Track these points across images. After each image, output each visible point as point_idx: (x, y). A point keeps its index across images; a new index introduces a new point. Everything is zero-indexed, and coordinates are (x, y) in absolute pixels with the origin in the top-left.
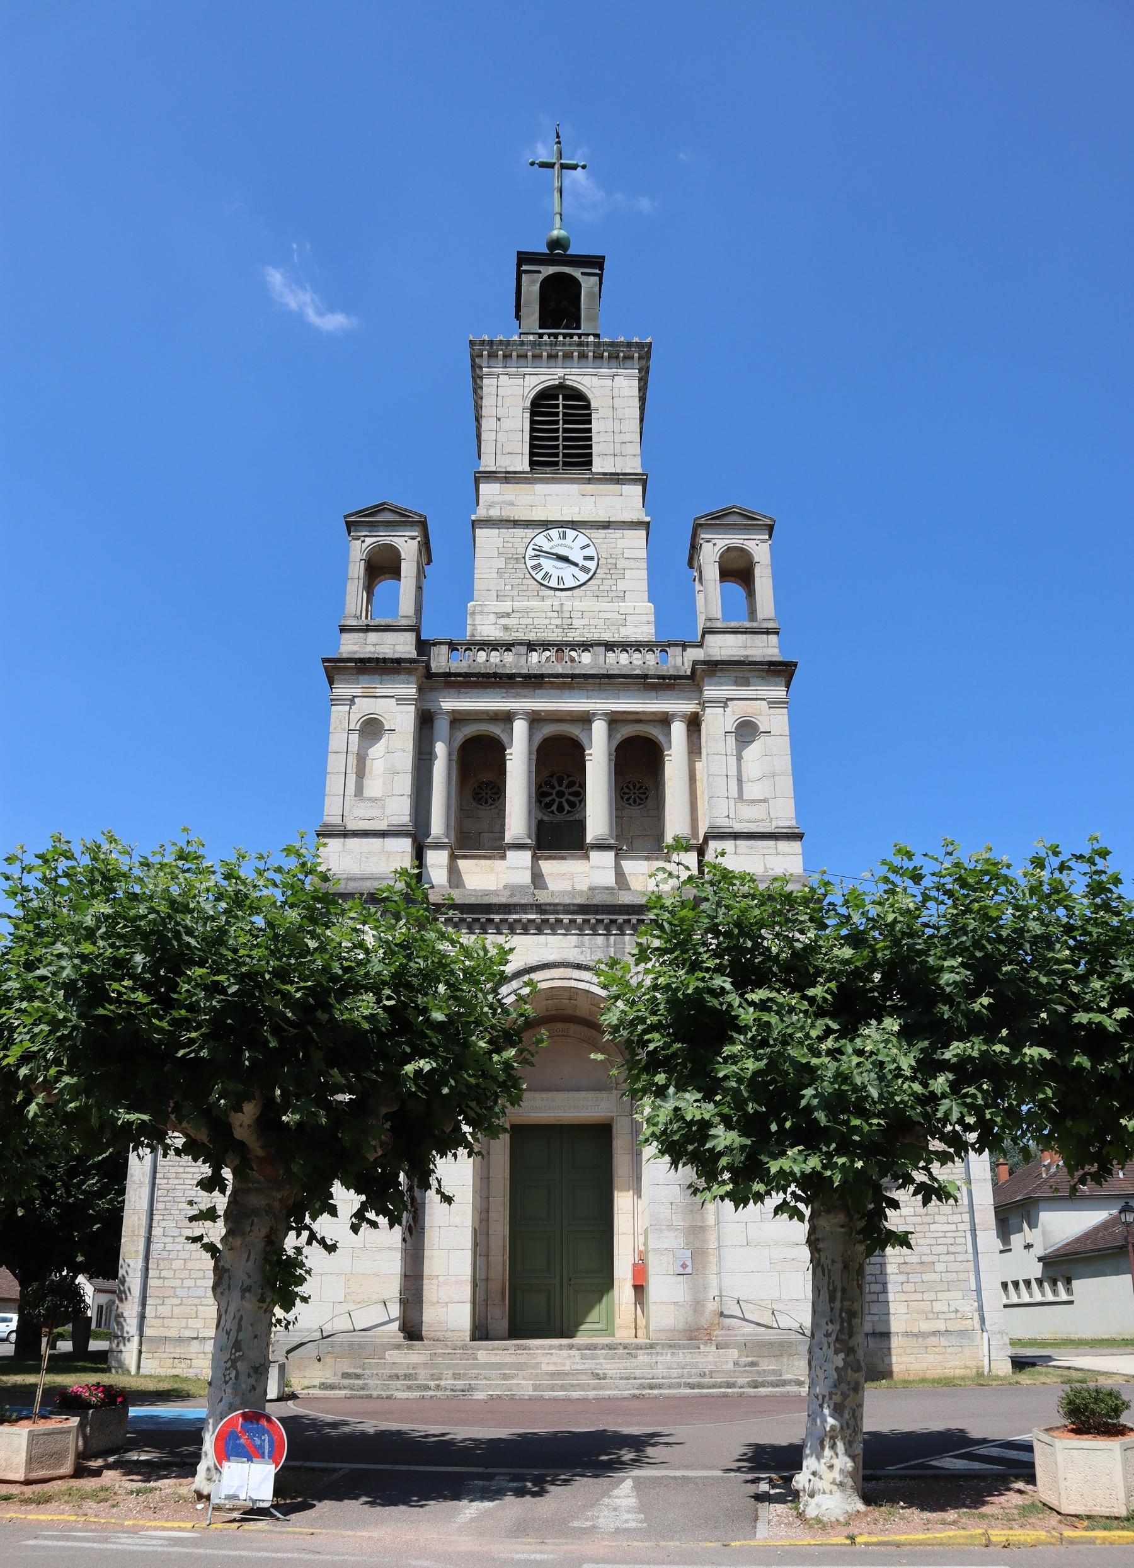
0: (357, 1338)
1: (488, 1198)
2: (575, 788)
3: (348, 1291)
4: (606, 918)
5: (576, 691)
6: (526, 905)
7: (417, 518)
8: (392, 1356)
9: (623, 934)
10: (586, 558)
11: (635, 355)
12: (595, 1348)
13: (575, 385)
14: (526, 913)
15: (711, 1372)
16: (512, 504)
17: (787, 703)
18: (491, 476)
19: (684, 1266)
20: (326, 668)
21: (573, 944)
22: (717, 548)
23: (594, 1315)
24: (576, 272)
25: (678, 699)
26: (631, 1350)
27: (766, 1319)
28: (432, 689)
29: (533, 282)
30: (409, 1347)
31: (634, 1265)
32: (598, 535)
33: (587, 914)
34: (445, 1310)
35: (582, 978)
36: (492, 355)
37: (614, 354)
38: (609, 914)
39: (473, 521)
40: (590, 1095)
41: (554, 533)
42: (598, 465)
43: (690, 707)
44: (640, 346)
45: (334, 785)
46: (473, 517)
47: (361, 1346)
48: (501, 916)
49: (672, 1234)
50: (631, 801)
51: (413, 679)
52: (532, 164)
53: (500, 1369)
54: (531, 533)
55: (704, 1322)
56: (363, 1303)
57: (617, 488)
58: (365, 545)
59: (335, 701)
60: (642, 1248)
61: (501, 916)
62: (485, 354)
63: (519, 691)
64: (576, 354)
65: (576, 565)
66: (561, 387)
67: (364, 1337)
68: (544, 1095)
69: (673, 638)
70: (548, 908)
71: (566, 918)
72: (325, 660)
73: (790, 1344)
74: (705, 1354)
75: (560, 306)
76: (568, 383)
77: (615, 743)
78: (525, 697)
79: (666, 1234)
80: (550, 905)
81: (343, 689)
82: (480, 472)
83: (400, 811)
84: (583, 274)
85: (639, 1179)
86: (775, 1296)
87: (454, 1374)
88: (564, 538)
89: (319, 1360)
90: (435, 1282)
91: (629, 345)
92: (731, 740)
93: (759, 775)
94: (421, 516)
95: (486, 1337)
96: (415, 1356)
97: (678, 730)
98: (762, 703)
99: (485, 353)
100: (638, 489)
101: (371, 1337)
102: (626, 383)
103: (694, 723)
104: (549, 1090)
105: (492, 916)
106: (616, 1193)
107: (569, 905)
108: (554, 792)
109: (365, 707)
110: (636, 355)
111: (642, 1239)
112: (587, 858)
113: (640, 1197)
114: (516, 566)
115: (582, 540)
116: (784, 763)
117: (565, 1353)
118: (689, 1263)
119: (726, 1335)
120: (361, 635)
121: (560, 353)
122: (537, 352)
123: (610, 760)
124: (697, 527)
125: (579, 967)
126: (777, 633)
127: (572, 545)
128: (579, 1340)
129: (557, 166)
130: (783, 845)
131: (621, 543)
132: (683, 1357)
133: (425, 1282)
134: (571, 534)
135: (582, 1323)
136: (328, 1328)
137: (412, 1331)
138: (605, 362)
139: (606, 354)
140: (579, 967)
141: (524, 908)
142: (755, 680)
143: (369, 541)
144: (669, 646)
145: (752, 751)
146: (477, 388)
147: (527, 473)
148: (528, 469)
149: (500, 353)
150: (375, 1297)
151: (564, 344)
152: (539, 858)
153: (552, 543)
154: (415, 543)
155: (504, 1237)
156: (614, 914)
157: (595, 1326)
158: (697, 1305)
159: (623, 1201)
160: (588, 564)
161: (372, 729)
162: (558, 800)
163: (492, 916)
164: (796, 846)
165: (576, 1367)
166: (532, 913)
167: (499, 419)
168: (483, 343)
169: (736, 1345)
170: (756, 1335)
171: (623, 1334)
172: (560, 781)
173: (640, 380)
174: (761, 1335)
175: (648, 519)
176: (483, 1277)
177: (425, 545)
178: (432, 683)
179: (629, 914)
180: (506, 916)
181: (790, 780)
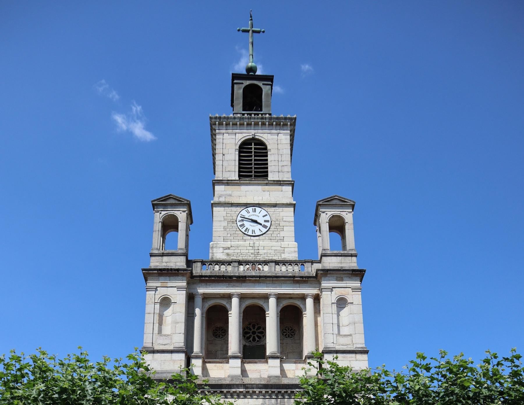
2: (261, 330)
4: (276, 391)
5: (261, 284)
6: (238, 385)
7: (186, 202)
10: (265, 221)
11: (288, 123)
13: (260, 138)
14: (239, 388)
16: (230, 195)
18: (220, 182)
20: (143, 273)
21: (261, 403)
22: (327, 216)
24: (260, 84)
25: (310, 287)
28: (193, 283)
33: (267, 389)
36: (221, 124)
37: (278, 123)
38: (278, 389)
39: (212, 204)
41: (250, 209)
42: (271, 177)
43: (315, 291)
44: (291, 119)
45: (148, 328)
46: (212, 202)
51: (185, 278)
52: (239, 30)
54: (239, 209)
59: (148, 289)
62: (217, 124)
64: (260, 123)
65: (261, 224)
66: (253, 139)
70: (249, 386)
71: (257, 391)
72: (143, 270)
76: (256, 137)
81: (152, 284)
82: (215, 180)
83: (179, 341)
84: (263, 84)
91: (286, 118)
92: (335, 306)
93: (347, 323)
94: (188, 201)
97: (309, 302)
98: (349, 289)
99: (217, 123)
100: (290, 188)
102: (284, 137)
103: (317, 299)
105: (223, 390)
107: (259, 384)
108: (251, 332)
109: (162, 292)
110: (289, 123)
112: (267, 362)
114: (232, 225)
115: (264, 212)
116: (359, 318)
120: (160, 257)
122: (242, 122)
124: (318, 206)
126: (356, 256)
129: (250, 32)
130: (359, 356)
131: (282, 214)
134: (258, 209)
138: (274, 127)
139: (274, 123)
141: (238, 386)
143: (163, 213)
144: (305, 262)
145: (344, 312)
148: (238, 179)
149: (224, 123)
151: (254, 118)
152: (244, 363)
154: (185, 214)
156: (280, 389)
160: (266, 224)
161: (166, 302)
163: (223, 390)
164: (365, 357)
166: (241, 388)
167: (224, 155)
168: (216, 118)
172: (254, 327)
173: (291, 136)
175: (294, 202)
177: (190, 215)
179: (287, 389)
180: (229, 390)
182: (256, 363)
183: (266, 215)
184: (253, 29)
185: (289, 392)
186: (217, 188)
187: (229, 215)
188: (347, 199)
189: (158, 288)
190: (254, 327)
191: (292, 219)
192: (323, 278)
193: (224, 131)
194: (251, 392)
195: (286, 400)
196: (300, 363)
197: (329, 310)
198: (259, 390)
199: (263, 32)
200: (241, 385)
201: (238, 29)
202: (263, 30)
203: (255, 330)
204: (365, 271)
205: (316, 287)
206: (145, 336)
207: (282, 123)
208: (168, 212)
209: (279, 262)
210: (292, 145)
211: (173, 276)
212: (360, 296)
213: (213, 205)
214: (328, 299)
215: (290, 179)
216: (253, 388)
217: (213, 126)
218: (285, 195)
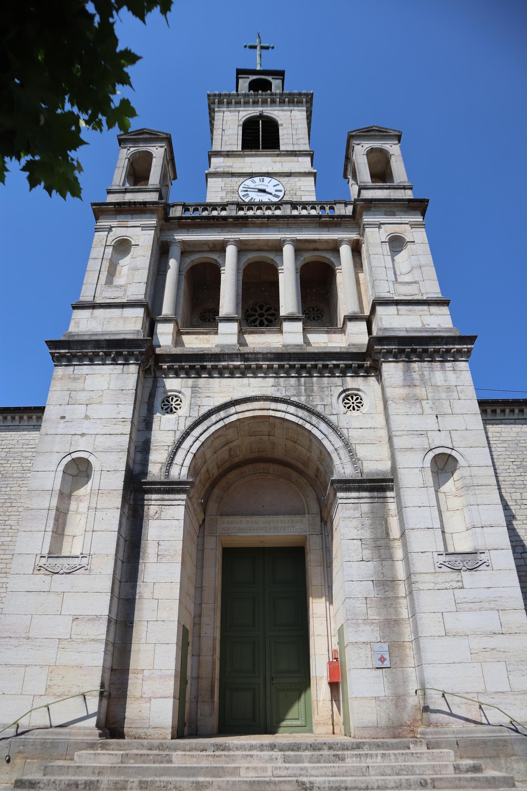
0: (50, 736)
1: (201, 604)
2: (272, 311)
3: (49, 683)
4: (297, 364)
5: (271, 229)
6: (232, 354)
7: (164, 136)
8: (85, 758)
9: (311, 376)
10: (276, 191)
11: (305, 100)
12: (299, 749)
13: (269, 115)
14: (233, 361)
15: (433, 780)
16: (231, 167)
17: (424, 225)
18: (218, 154)
19: (382, 659)
20: (94, 210)
21: (271, 384)
22: (364, 148)
23: (293, 712)
24: (269, 78)
25: (344, 232)
26: (336, 751)
27: (475, 714)
28: (169, 229)
29: (245, 82)
30: (103, 747)
31: (330, 663)
32: (285, 180)
33: (282, 361)
34: (148, 705)
35: (279, 408)
36: (221, 103)
37: (291, 100)
38: (300, 360)
39: (207, 174)
40: (287, 518)
41: (257, 179)
42: (282, 148)
43: (354, 236)
44: (306, 95)
45: (90, 278)
46: (206, 172)
47: (54, 745)
48: (212, 364)
49: (368, 628)
50: (312, 318)
51: (155, 216)
52: (245, 47)
53: (194, 775)
54: (241, 179)
55: (406, 718)
56: (63, 697)
57: (295, 159)
58: (129, 152)
59: (97, 230)
60: (336, 647)
61: (212, 364)
62: (216, 101)
63: (230, 229)
64: (269, 100)
65: (271, 194)
66: (261, 116)
67: (59, 734)
68: (249, 519)
69: (337, 199)
70: (250, 356)
71: (265, 364)
72: (93, 204)
73: (505, 742)
74: (418, 756)
75: (260, 85)
76: (264, 114)
77: (300, 264)
78: (235, 232)
79: (363, 627)
80: (252, 354)
81: (104, 223)
82: (211, 152)
83: (138, 290)
84: (272, 78)
85: (330, 588)
86: (480, 688)
87: (140, 782)
88: (263, 181)
89: (8, 761)
90: (140, 676)
91: (300, 94)
92: (386, 247)
93: (408, 269)
94: (167, 134)
95: (195, 734)
96: (108, 756)
97: (345, 251)
98: (405, 225)
99: (216, 100)
100: (309, 159)
101: (67, 734)
102: (299, 115)
103: (356, 249)
104: (253, 514)
105: (205, 364)
106: (311, 599)
107: (267, 353)
108: (257, 314)
109: (118, 233)
110: (304, 100)
111: (335, 640)
112: (281, 331)
113: (331, 603)
114: (232, 195)
115: (274, 182)
116: (427, 259)
117: (266, 754)
118: (387, 656)
119: (436, 733)
120: (121, 195)
121: (260, 100)
122: (247, 99)
123: (297, 273)
124: (351, 137)
125: (276, 400)
126: (411, 189)
127: (268, 184)
128: (281, 738)
129: (258, 48)
130: (434, 309)
131: (299, 184)
132: (395, 759)
133: (131, 676)
134: (267, 179)
135: (283, 720)
136: (24, 723)
137: (112, 726)
138: (286, 104)
139: (287, 99)
140: (276, 400)
141: (231, 356)
142: (398, 211)
143: (132, 149)
144: (335, 204)
145: (402, 257)
146: (212, 119)
147: (240, 151)
148: (240, 148)
149: (225, 100)
150: (76, 690)
151: (262, 95)
152: (244, 333)
153: (256, 184)
154: (163, 150)
155: (214, 639)
156: (304, 361)
157: (295, 723)
158: (398, 699)
159: (317, 607)
160: (278, 193)
161: (123, 246)
162: (259, 319)
163: (205, 364)
164: (445, 310)
165: (278, 772)
166: (237, 361)
167: (224, 130)
168: (215, 95)
169: (449, 745)
170: (467, 732)
171: (321, 732)
172: (261, 307)
173: (307, 111)
174: (472, 732)
175: (315, 171)
176: (195, 675)
177: (170, 158)
178: (167, 223)
179: (316, 361)
180: (217, 364)
181: (433, 270)
182: (263, 333)
183: (278, 185)
184: (262, 44)
185: (320, 366)
186: (214, 160)
187: (229, 185)
188: (390, 130)
189: (113, 229)
190: (261, 307)
191: (313, 188)
192: (364, 213)
193: (225, 109)
194: (253, 366)
195: (315, 379)
196: (335, 333)
197: (379, 250)
198: (268, 363)
199: (273, 48)
200: (237, 354)
201: (245, 44)
202: (272, 46)
203: (263, 311)
204: (428, 201)
205: (354, 230)
206: (84, 288)
207: (296, 99)
208: (139, 148)
209: (298, 204)
210: (309, 138)
211: (137, 214)
212: (425, 234)
213: (207, 176)
214: (375, 237)
215: (308, 149)
216: (258, 361)
217: (212, 106)
218: (304, 164)
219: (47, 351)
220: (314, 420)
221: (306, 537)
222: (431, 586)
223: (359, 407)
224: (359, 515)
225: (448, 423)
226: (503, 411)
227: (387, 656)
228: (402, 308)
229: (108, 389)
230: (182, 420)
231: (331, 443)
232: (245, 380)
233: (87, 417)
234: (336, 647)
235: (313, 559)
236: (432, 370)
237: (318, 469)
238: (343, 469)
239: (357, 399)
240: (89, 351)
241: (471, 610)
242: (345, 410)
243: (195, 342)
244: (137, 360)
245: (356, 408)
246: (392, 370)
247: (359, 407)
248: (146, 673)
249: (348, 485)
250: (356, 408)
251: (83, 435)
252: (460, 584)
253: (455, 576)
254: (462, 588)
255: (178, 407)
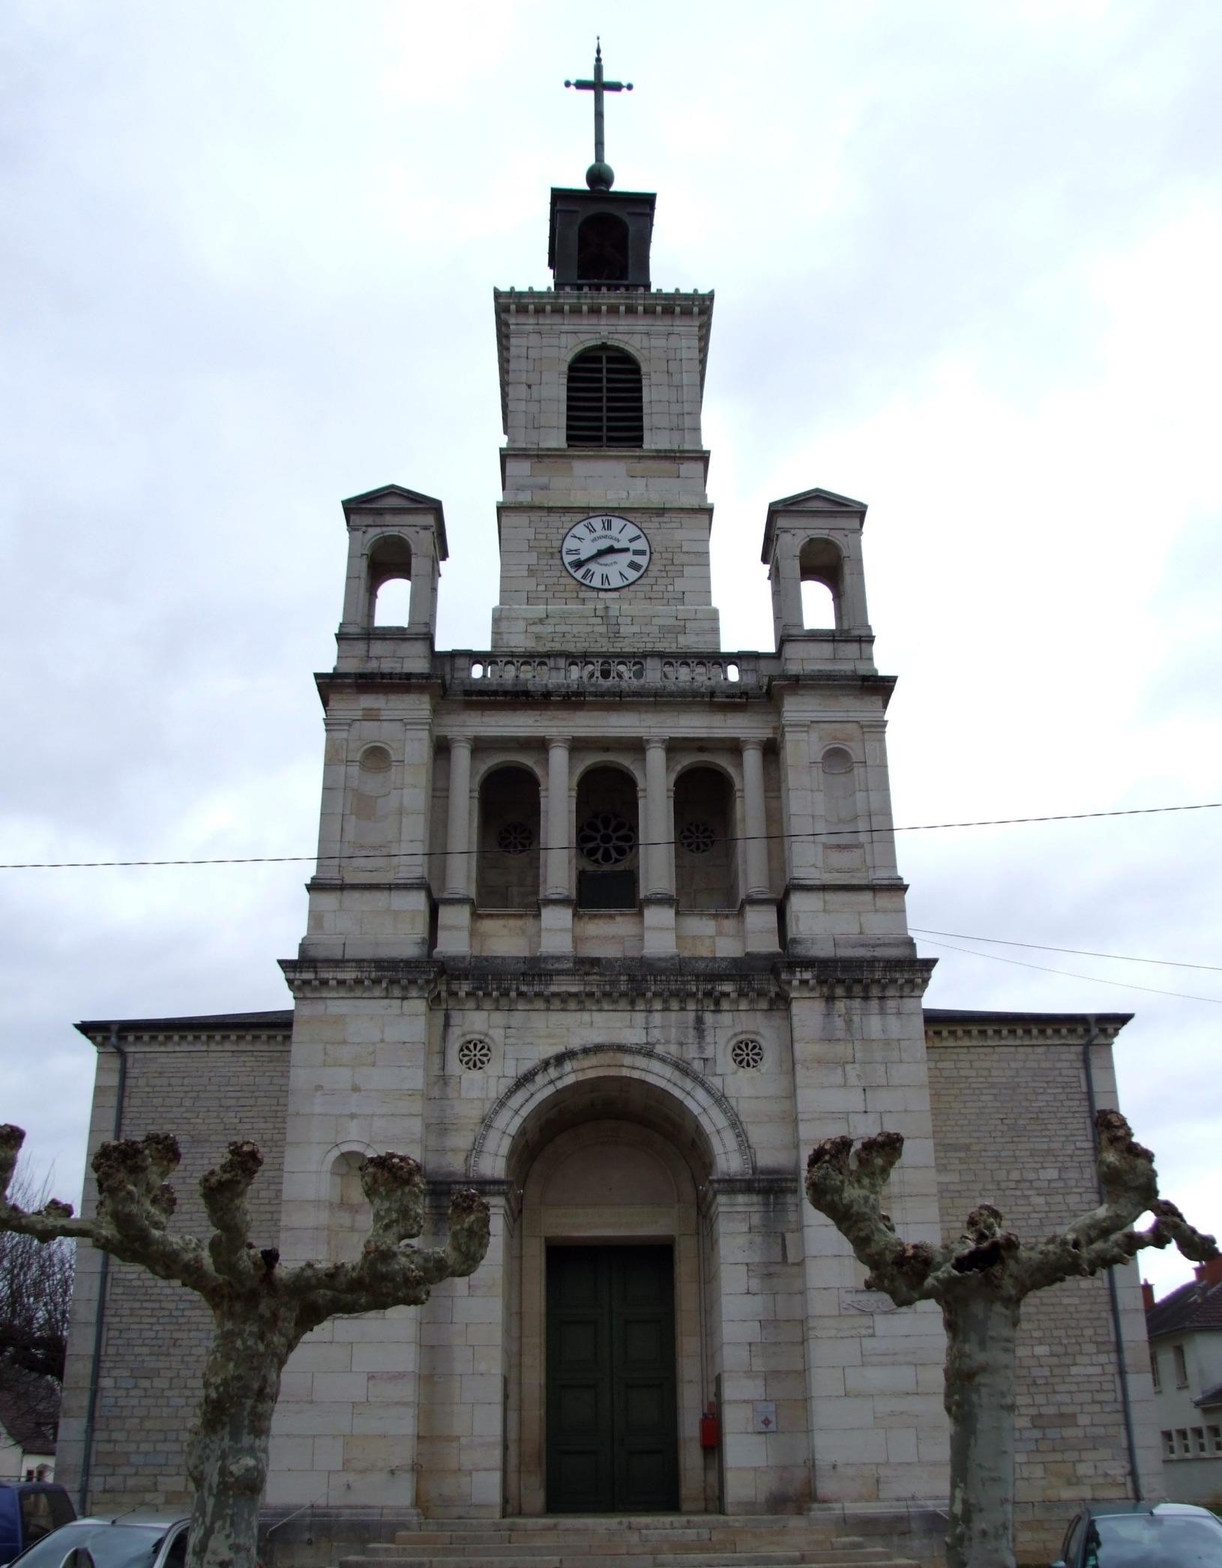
35: (637, 1065)
65: (626, 550)
103: (771, 750)
127: (619, 536)
183: (638, 537)
219: (280, 974)
220: (688, 1084)
221: (672, 1239)
222: (833, 1333)
223: (755, 1061)
224: (746, 1229)
225: (883, 1100)
226: (998, 1032)
227: (772, 1418)
228: (830, 897)
229: (382, 1041)
230: (493, 1082)
231: (712, 1121)
232: (586, 1017)
233: (356, 1089)
234: (712, 1398)
235: (684, 1269)
236: (865, 1013)
237: (694, 1141)
238: (728, 1160)
239: (754, 1048)
240: (349, 975)
241: (882, 1364)
242: (734, 1066)
243: (505, 940)
244: (421, 989)
245: (752, 1063)
246: (807, 1013)
247: (755, 1061)
248: (463, 1441)
249: (733, 1185)
250: (752, 1063)
251: (353, 1116)
252: (870, 1331)
253: (865, 1321)
254: (873, 1336)
255: (485, 1059)
